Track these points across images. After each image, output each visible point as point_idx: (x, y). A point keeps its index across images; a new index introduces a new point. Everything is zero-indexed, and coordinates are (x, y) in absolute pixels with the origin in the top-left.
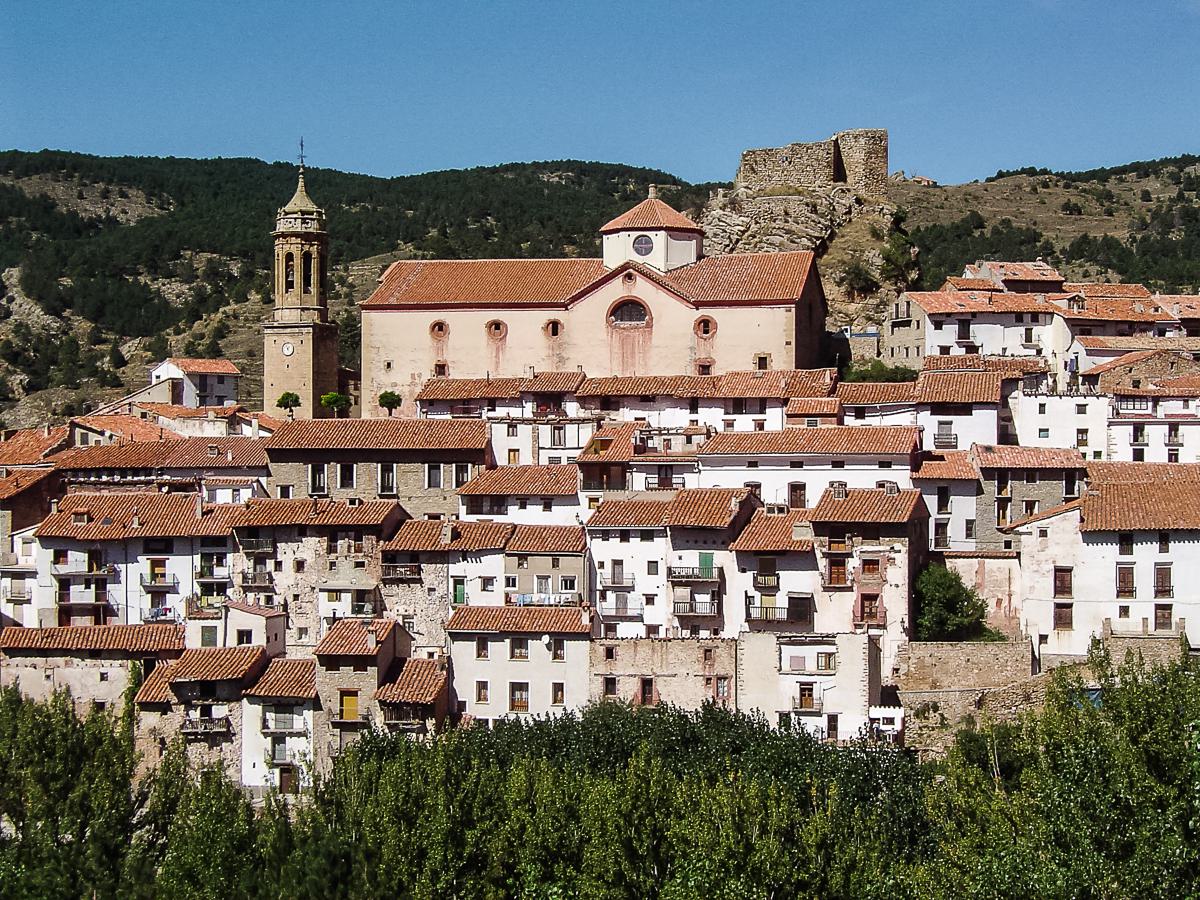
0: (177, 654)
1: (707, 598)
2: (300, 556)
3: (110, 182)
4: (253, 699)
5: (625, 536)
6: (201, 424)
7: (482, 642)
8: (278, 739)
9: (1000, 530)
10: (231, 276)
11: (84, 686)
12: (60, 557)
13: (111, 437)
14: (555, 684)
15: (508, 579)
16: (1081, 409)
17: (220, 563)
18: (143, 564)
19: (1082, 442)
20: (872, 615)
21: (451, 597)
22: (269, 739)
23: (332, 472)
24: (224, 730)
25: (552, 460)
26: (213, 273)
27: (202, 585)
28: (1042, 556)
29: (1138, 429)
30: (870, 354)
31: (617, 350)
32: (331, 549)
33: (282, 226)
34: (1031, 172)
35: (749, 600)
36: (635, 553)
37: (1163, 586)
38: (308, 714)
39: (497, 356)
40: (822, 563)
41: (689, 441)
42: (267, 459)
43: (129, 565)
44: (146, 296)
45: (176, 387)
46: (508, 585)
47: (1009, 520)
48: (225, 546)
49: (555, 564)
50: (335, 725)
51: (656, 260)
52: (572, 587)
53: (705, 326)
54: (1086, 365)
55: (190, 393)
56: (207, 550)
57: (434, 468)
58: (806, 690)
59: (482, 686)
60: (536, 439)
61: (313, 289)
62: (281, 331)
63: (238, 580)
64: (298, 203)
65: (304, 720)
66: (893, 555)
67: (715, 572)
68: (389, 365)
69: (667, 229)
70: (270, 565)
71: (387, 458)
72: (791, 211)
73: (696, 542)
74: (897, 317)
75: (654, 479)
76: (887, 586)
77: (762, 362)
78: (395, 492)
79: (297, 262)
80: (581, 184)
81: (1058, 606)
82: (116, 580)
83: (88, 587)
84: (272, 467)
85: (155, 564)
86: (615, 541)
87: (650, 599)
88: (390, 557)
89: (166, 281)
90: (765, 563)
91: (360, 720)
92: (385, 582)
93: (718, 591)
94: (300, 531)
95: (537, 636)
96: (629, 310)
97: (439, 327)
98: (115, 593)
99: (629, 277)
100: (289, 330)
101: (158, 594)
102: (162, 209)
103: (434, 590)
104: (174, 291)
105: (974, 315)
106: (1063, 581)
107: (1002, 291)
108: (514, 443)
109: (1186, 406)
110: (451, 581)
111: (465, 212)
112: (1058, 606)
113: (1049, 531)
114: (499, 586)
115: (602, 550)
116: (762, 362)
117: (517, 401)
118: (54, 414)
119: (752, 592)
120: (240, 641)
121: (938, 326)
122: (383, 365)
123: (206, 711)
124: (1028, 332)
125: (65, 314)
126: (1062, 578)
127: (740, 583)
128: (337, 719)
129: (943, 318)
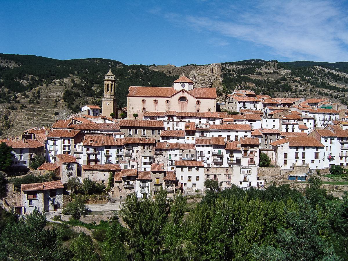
0: (120, 170)
1: (219, 158)
2: (137, 150)
3: (7, 59)
4: (138, 180)
5: (203, 146)
6: (98, 120)
7: (182, 168)
8: (143, 188)
9: (265, 145)
10: (36, 80)
11: (100, 177)
12: (88, 149)
13: (81, 122)
14: (197, 176)
15: (180, 154)
16: (274, 121)
17: (120, 151)
18: (105, 151)
19: (274, 127)
20: (252, 162)
21: (168, 158)
22: (141, 188)
23: (133, 131)
24: (132, 186)
25: (176, 129)
26: (32, 79)
27: (117, 155)
28: (282, 151)
29: (287, 125)
30: (224, 108)
31: (180, 107)
32: (144, 148)
33: (106, 78)
34: (193, 65)
35: (228, 159)
36: (205, 150)
37: (303, 157)
38: (149, 183)
39: (156, 107)
40: (243, 152)
41: (206, 126)
42: (119, 128)
43: (102, 151)
44: (19, 84)
45: (89, 111)
46: (180, 156)
47: (267, 143)
48: (122, 147)
49: (190, 152)
50: (155, 185)
51: (186, 88)
52: (193, 156)
53: (198, 102)
54: (269, 112)
55: (91, 112)
56: (118, 148)
57: (153, 130)
58: (245, 177)
59: (182, 177)
60: (173, 125)
61: (113, 91)
62: (106, 100)
63: (124, 154)
64: (110, 73)
65: (148, 184)
66: (256, 151)
67: (221, 154)
68: (133, 108)
69: (188, 83)
70: (131, 151)
71: (144, 128)
72: (205, 79)
73: (218, 148)
74: (230, 101)
75: (200, 134)
76: (255, 157)
77: (209, 110)
78: (145, 135)
79: (110, 85)
80: (103, 63)
81: (284, 160)
82: (99, 154)
83: (93, 156)
84: (121, 130)
85: (107, 151)
86: (201, 147)
87: (208, 159)
88: (156, 150)
89: (23, 81)
90: (231, 152)
91: (160, 184)
92: (155, 155)
93: (222, 157)
94: (138, 145)
95: (194, 167)
96: (183, 99)
97: (144, 100)
98: (99, 157)
99: (183, 92)
100: (108, 100)
101: (108, 157)
102: (19, 65)
103: (165, 156)
104: (25, 83)
105: (246, 101)
106: (285, 156)
107: (245, 96)
108: (169, 126)
109: (294, 121)
110: (168, 155)
111: (82, 68)
112: (284, 160)
113: (283, 146)
114: (178, 156)
115: (199, 149)
116: (209, 110)
117: (164, 117)
118: (6, 109)
119: (229, 157)
120: (132, 168)
121: (239, 103)
122: (132, 108)
123: (128, 182)
124: (255, 105)
125: (2, 87)
126: (285, 155)
127: (226, 156)
128: (155, 184)
129: (240, 102)
